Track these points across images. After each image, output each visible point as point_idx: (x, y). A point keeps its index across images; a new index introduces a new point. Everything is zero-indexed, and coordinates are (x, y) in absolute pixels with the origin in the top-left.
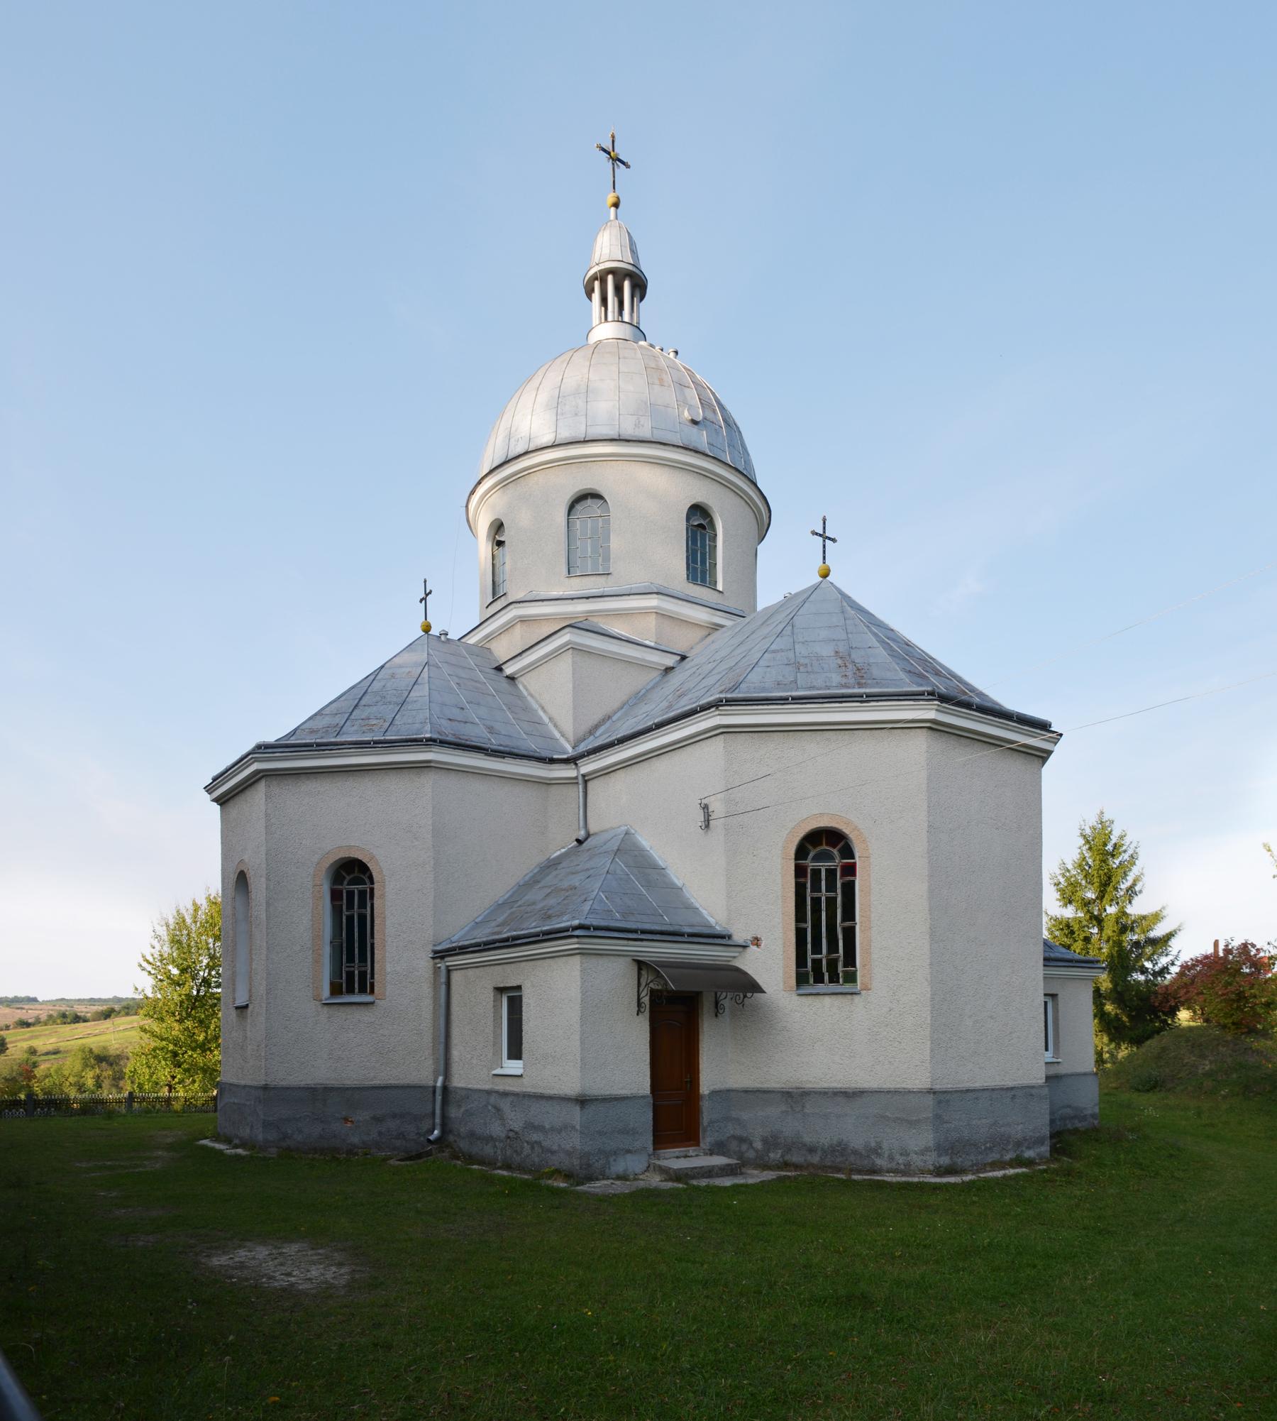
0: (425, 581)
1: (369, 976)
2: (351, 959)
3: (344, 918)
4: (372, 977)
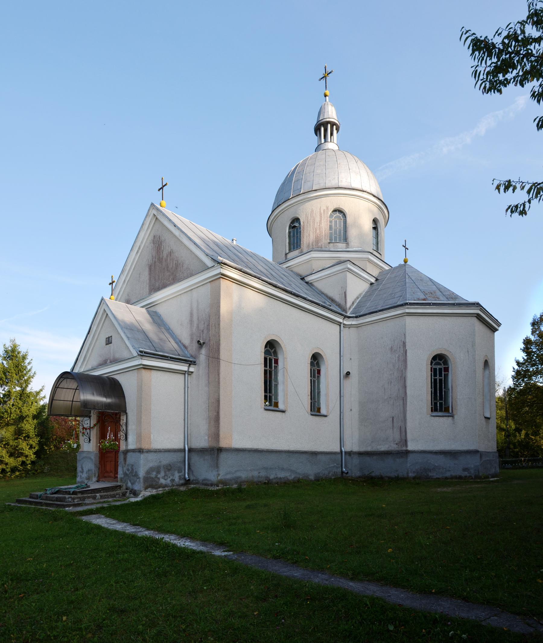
0: (405, 241)
1: (433, 374)
2: (441, 380)
3: (444, 399)
4: (431, 374)
